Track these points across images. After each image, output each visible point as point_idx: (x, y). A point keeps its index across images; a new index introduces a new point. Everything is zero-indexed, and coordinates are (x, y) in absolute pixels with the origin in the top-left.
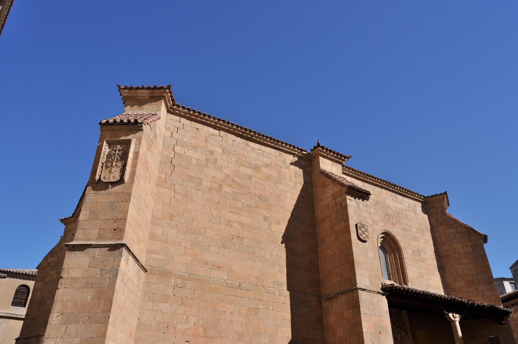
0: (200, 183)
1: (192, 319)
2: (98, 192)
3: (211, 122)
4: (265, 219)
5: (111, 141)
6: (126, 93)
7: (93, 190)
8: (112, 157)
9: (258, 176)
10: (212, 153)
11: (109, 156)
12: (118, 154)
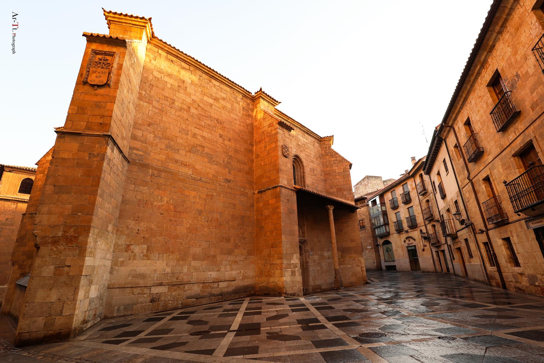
0: (173, 103)
1: (165, 199)
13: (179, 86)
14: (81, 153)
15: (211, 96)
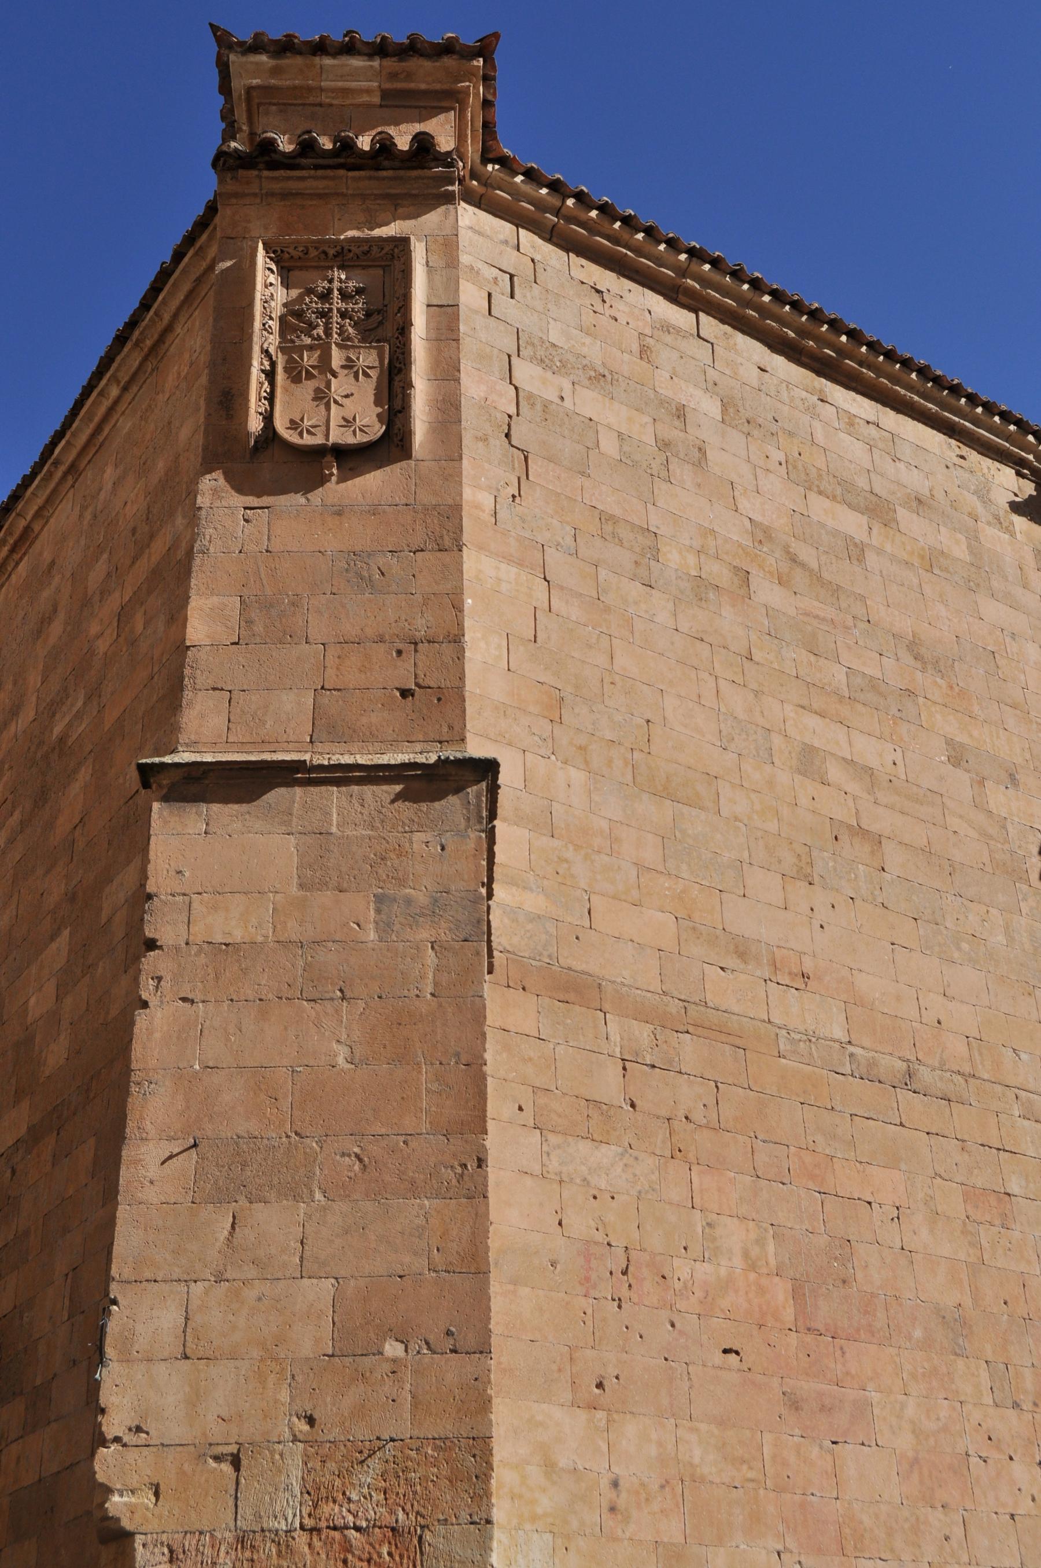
0: (655, 554)
1: (734, 1235)
2: (266, 500)
3: (659, 261)
4: (957, 756)
5: (296, 245)
6: (252, 71)
7: (240, 490)
8: (312, 326)
9: (888, 548)
10: (681, 413)
11: (293, 321)
12: (343, 315)
13: (664, 445)
14: (326, 897)
15: (845, 493)
